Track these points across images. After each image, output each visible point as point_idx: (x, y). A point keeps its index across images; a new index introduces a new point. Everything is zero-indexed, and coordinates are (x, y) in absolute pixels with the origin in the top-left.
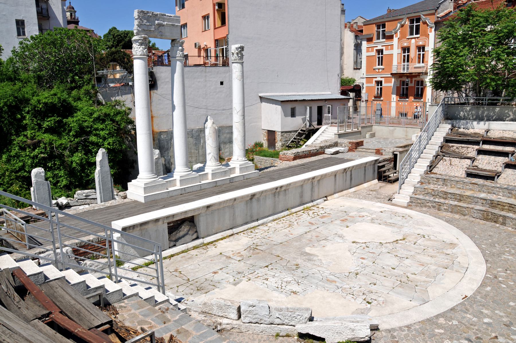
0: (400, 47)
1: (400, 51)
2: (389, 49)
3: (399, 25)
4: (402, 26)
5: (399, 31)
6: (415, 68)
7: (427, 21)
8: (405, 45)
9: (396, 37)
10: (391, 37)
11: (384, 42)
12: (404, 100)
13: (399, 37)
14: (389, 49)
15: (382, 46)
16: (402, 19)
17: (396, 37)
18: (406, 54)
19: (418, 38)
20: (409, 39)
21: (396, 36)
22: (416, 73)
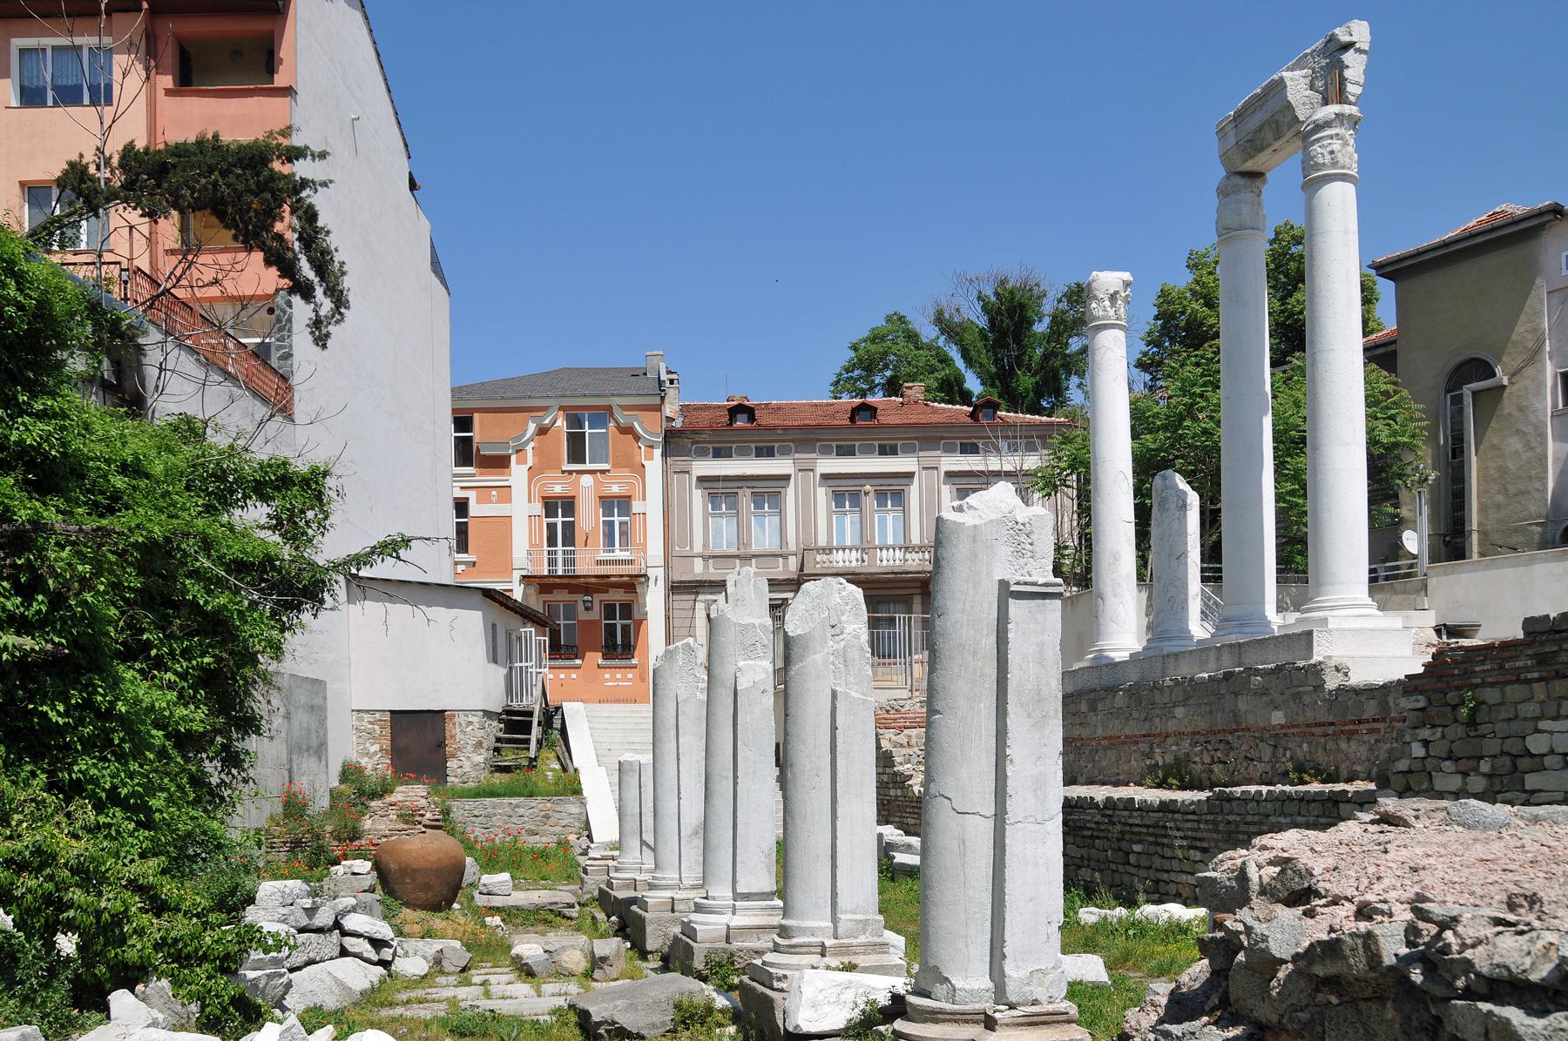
0: (536, 495)
1: (538, 508)
2: (494, 499)
3: (532, 427)
4: (542, 431)
5: (532, 444)
6: (599, 563)
7: (635, 424)
8: (558, 490)
9: (518, 463)
10: (501, 463)
11: (473, 475)
12: (568, 663)
13: (530, 463)
14: (494, 499)
15: (462, 488)
16: (545, 409)
17: (518, 463)
18: (559, 520)
19: (603, 472)
20: (570, 472)
21: (522, 461)
22: (622, 576)
